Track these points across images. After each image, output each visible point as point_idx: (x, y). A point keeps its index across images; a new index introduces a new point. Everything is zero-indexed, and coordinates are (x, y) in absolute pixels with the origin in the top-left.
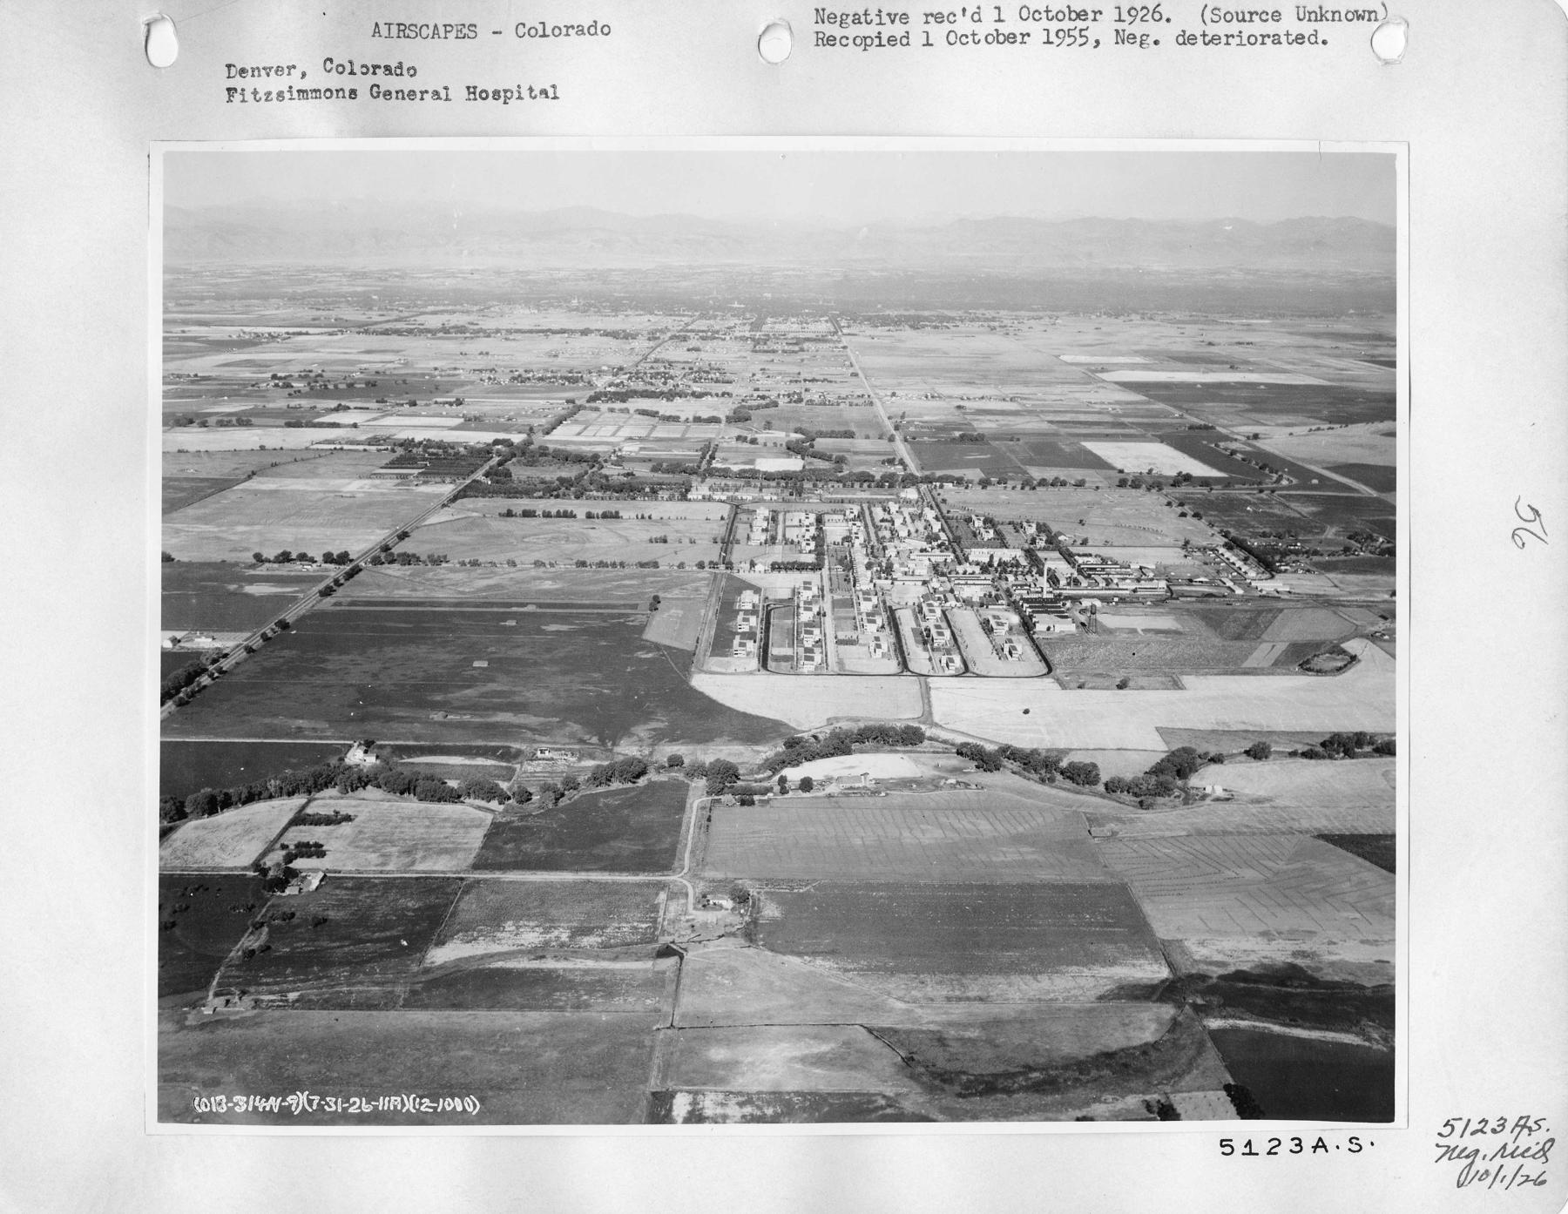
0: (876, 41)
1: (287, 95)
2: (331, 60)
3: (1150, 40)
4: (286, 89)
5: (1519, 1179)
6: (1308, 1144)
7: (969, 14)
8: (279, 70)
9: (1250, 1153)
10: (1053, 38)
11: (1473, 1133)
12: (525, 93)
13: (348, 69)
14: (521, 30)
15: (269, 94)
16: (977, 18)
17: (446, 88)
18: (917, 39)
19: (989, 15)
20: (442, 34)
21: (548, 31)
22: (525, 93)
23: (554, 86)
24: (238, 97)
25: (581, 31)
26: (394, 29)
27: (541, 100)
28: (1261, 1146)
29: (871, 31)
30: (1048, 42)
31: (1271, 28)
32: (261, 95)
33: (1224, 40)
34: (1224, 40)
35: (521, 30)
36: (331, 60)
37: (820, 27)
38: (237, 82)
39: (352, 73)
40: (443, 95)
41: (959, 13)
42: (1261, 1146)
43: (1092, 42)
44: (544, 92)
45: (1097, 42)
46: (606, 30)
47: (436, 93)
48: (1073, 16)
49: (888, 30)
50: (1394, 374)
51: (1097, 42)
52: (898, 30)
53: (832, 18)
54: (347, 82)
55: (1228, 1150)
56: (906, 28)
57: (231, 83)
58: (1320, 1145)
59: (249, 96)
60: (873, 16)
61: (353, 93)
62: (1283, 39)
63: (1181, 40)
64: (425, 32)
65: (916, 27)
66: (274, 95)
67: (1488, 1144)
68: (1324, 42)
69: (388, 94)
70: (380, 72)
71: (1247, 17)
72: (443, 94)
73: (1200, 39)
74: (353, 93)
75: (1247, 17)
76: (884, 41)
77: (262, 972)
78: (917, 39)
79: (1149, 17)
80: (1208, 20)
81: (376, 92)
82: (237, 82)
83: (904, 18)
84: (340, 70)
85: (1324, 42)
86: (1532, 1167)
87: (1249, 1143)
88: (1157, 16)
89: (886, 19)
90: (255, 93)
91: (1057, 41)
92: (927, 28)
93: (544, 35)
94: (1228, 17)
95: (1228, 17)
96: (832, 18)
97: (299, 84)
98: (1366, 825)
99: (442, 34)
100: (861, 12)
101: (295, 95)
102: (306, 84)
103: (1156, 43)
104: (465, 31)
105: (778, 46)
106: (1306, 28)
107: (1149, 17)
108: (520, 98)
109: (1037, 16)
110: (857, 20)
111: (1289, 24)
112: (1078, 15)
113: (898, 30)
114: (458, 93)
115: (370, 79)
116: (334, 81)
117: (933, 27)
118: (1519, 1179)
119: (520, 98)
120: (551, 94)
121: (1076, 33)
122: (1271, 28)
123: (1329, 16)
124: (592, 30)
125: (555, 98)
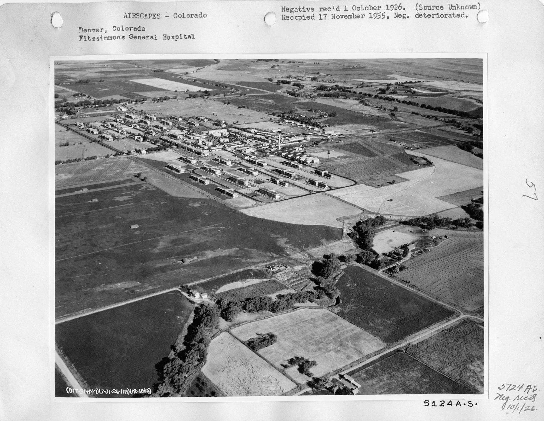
0: (437, 16)
1: (100, 39)
2: (115, 27)
3: (406, 16)
4: (100, 37)
5: (524, 409)
6: (454, 403)
7: (335, 8)
8: (97, 30)
9: (434, 406)
10: (373, 16)
11: (510, 390)
12: (183, 37)
13: (121, 29)
14: (176, 16)
15: (94, 38)
16: (338, 9)
17: (155, 35)
18: (317, 17)
19: (342, 9)
20: (148, 17)
21: (185, 16)
22: (183, 37)
23: (193, 35)
24: (83, 39)
25: (196, 16)
26: (131, 15)
27: (189, 39)
28: (438, 403)
29: (301, 14)
30: (371, 18)
31: (441, 12)
32: (91, 38)
33: (432, 16)
34: (432, 16)
35: (176, 16)
36: (115, 27)
37: (284, 13)
38: (83, 34)
39: (123, 30)
40: (154, 38)
41: (332, 8)
42: (438, 403)
43: (386, 17)
44: (189, 37)
45: (388, 17)
46: (205, 16)
47: (152, 37)
48: (371, 8)
49: (307, 14)
50: (482, 237)
51: (388, 17)
52: (310, 14)
53: (287, 10)
54: (121, 33)
55: (427, 404)
56: (313, 13)
57: (81, 34)
58: (458, 403)
59: (87, 39)
60: (301, 9)
61: (123, 37)
62: (452, 16)
63: (417, 16)
64: (142, 16)
65: (317, 13)
66: (96, 39)
67: (512, 394)
68: (467, 17)
69: (135, 37)
70: (132, 29)
71: (432, 8)
72: (154, 37)
73: (423, 16)
74: (123, 37)
75: (432, 8)
76: (305, 18)
77: (93, 354)
78: (317, 17)
79: (397, 8)
80: (418, 9)
81: (131, 37)
82: (83, 34)
83: (313, 9)
84: (119, 29)
85: (467, 17)
86: (529, 403)
87: (434, 402)
88: (400, 8)
89: (306, 10)
90: (89, 38)
91: (374, 17)
92: (320, 13)
93: (184, 17)
94: (428, 8)
95: (428, 8)
96: (287, 10)
97: (104, 35)
98: (480, 99)
99: (148, 17)
100: (298, 8)
101: (103, 39)
102: (107, 35)
103: (408, 17)
104: (156, 16)
105: (271, 19)
106: (451, 12)
107: (397, 8)
108: (181, 39)
109: (358, 9)
110: (296, 10)
111: (446, 11)
112: (373, 8)
113: (310, 14)
114: (160, 37)
115: (129, 32)
116: (116, 33)
117: (323, 12)
118: (524, 409)
119: (181, 39)
120: (192, 37)
121: (381, 14)
122: (441, 12)
123: (460, 7)
124: (200, 16)
125: (193, 38)
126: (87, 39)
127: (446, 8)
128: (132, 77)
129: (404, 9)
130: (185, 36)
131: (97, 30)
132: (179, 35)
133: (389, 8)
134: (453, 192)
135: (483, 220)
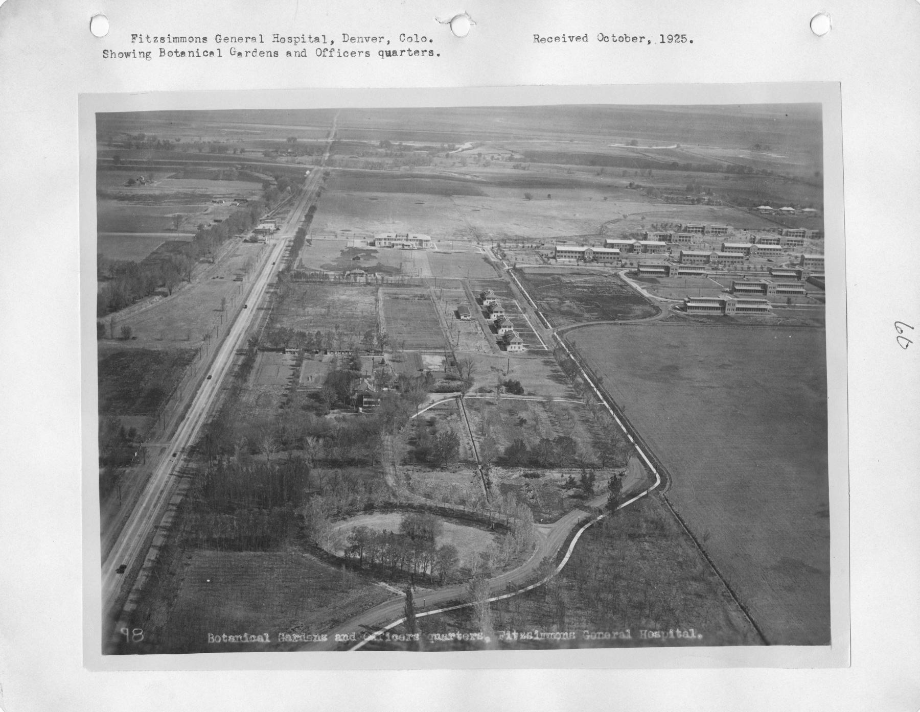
1: (167, 40)
8: (374, 39)
12: (307, 39)
24: (138, 40)
66: (159, 39)
73: (611, 39)
74: (205, 39)
126: (144, 39)
127: (268, 39)
128: (206, 164)
129: (691, 42)
130: (148, 37)
131: (577, 39)
132: (300, 36)
133: (666, 40)
134: (458, 201)
135: (822, 209)
